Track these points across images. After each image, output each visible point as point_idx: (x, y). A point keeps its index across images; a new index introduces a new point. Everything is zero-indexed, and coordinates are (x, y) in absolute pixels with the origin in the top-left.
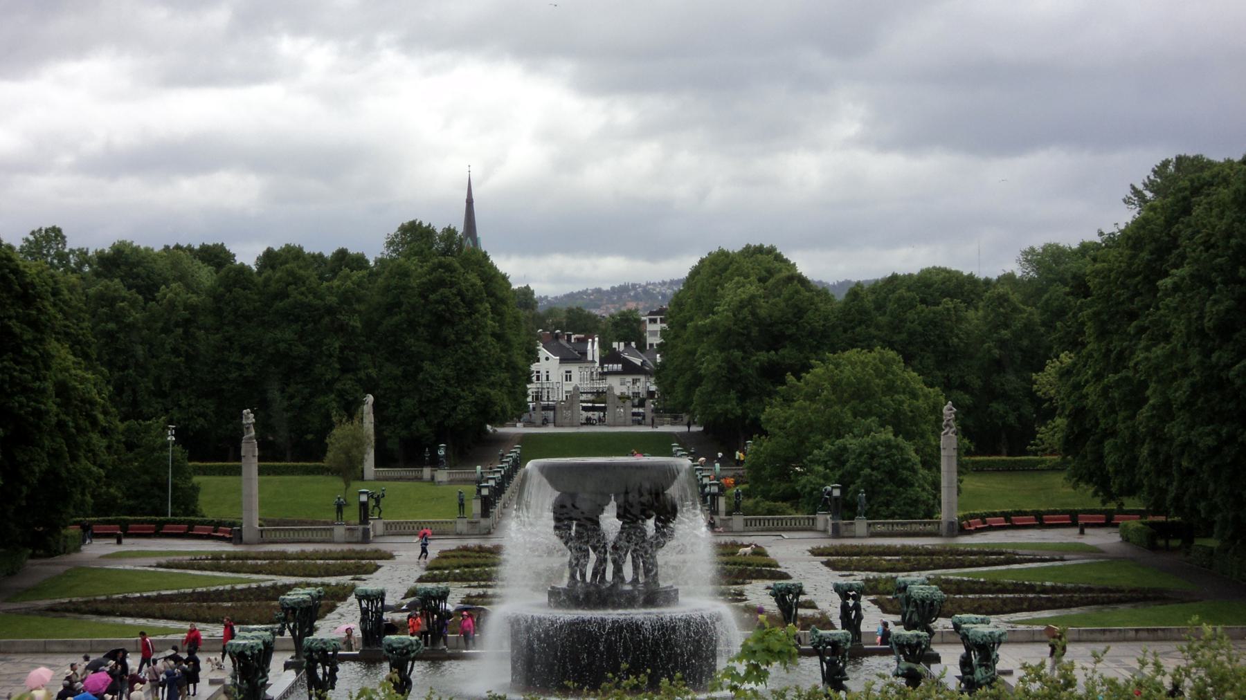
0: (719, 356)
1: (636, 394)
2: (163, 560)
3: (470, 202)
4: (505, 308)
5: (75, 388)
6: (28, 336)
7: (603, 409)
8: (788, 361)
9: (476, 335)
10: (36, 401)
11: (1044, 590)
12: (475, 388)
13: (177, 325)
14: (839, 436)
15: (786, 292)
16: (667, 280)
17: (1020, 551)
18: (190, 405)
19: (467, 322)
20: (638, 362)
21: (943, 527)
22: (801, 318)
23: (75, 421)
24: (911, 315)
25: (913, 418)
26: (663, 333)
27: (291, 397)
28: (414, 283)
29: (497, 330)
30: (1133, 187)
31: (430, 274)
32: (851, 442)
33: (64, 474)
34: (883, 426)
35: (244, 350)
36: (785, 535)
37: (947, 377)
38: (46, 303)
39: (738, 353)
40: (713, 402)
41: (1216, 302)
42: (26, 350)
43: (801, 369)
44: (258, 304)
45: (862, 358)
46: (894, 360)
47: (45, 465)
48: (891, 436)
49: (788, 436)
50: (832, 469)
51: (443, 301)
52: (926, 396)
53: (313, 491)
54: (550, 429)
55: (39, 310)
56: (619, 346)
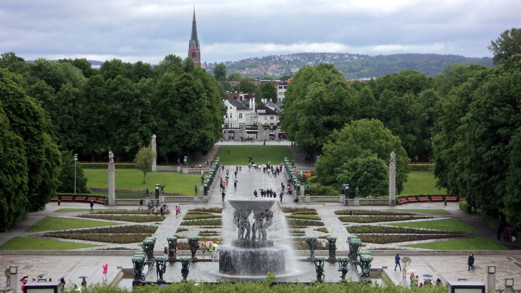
0: (307, 118)
1: (272, 124)
2: (81, 214)
3: (194, 23)
4: (212, 94)
5: (52, 151)
6: (36, 132)
7: (256, 133)
8: (335, 121)
9: (200, 107)
10: (39, 157)
11: (419, 232)
12: (200, 130)
13: (70, 102)
14: (355, 157)
15: (336, 90)
16: (291, 54)
17: (417, 213)
18: (76, 137)
19: (197, 101)
20: (273, 109)
21: (390, 202)
22: (342, 101)
23: (51, 163)
24: (390, 100)
25: (386, 149)
26: (285, 93)
27: (120, 134)
28: (174, 84)
29: (210, 105)
30: (493, 42)
31: (181, 80)
32: (360, 160)
33: (48, 183)
34: (373, 153)
35: (100, 113)
36: (326, 204)
37: (406, 128)
38: (42, 120)
39: (314, 117)
40: (304, 138)
41: (481, 128)
42: (35, 138)
43: (339, 126)
44: (106, 93)
45: (366, 123)
46: (379, 124)
47: (41, 180)
48: (376, 158)
49: (334, 156)
50: (351, 171)
51: (187, 92)
52: (393, 140)
53: (132, 177)
55: (39, 122)
56: (264, 101)
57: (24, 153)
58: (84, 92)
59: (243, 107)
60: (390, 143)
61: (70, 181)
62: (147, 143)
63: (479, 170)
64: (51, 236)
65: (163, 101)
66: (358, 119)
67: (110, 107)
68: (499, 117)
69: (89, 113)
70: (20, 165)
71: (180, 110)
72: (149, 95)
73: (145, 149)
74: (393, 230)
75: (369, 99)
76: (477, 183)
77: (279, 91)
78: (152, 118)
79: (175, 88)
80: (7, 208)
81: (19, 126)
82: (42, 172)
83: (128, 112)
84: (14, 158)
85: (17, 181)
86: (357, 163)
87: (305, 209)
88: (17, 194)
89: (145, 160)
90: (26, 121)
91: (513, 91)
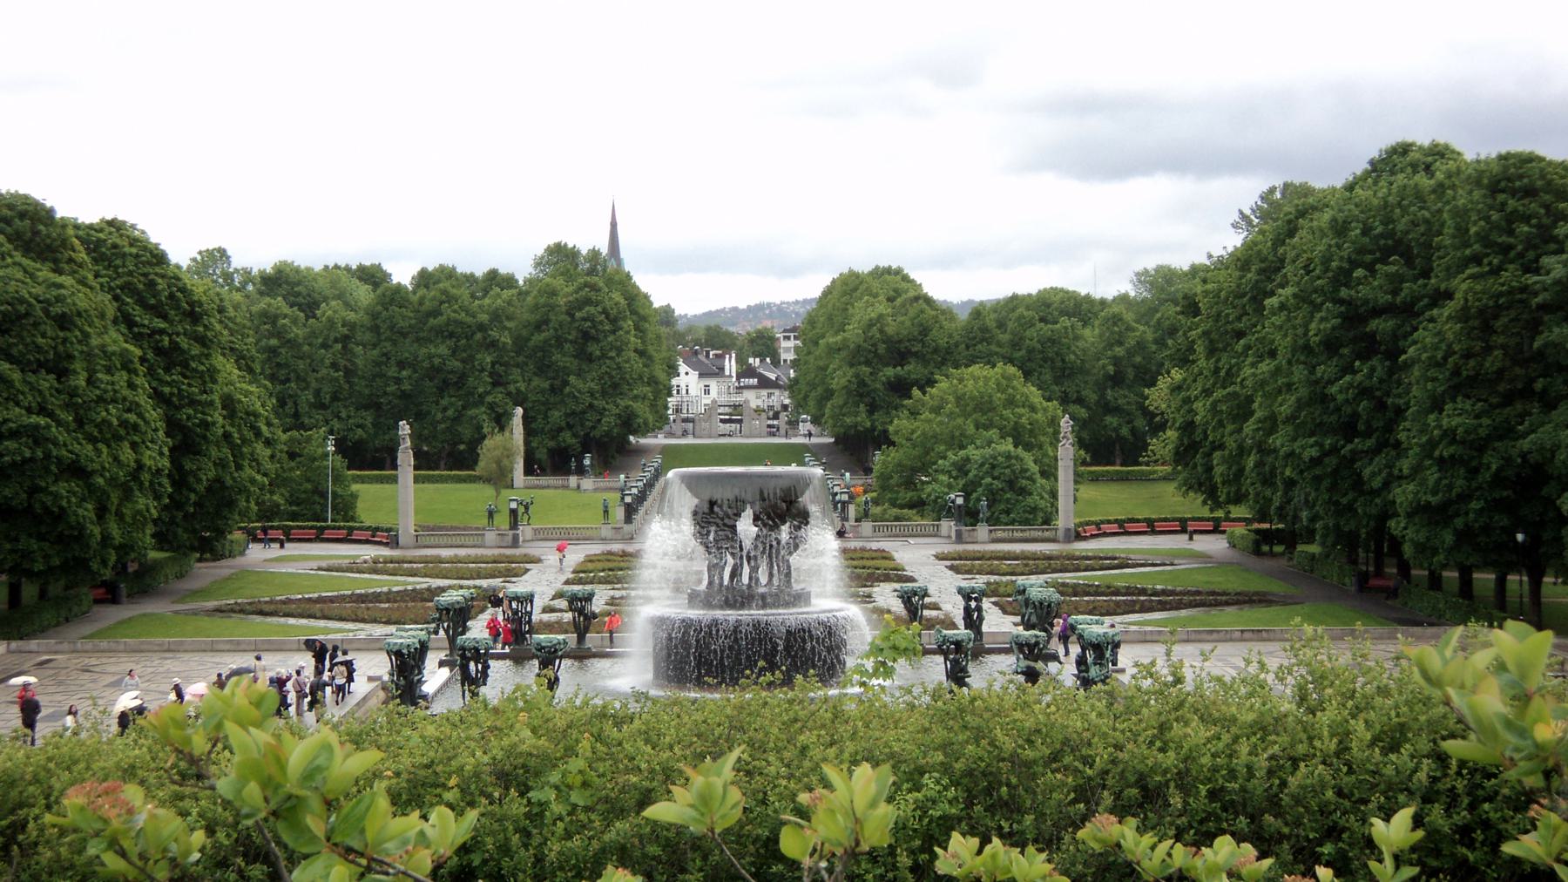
0: (851, 372)
1: (771, 408)
2: (324, 564)
3: (614, 225)
5: (240, 401)
7: (740, 421)
9: (619, 351)
13: (336, 341)
14: (962, 447)
15: (912, 312)
19: (611, 338)
20: (773, 377)
21: (1060, 534)
23: (239, 431)
25: (1031, 431)
27: (445, 409)
29: (640, 347)
30: (1241, 212)
32: (973, 453)
33: (229, 482)
35: (401, 365)
36: (911, 541)
39: (866, 369)
48: (1011, 447)
50: (955, 478)
54: (690, 440)
55: (205, 326)
56: (754, 362)
57: (144, 389)
58: (366, 320)
59: (711, 371)
60: (1039, 416)
61: (317, 498)
62: (501, 421)
63: (1318, 428)
64: (233, 611)
65: (538, 338)
66: (967, 366)
67: (423, 351)
68: (1370, 289)
69: (377, 364)
70: (132, 417)
71: (575, 357)
72: (508, 324)
73: (498, 438)
74: (1092, 590)
75: (984, 330)
76: (1315, 462)
77: (784, 344)
78: (515, 374)
79: (564, 309)
80: (97, 530)
81: (150, 336)
82: (214, 452)
83: (463, 361)
84: (114, 401)
85: (122, 458)
86: (967, 460)
87: (863, 549)
88: (127, 495)
89: (498, 462)
90: (171, 322)
91: (1402, 225)
